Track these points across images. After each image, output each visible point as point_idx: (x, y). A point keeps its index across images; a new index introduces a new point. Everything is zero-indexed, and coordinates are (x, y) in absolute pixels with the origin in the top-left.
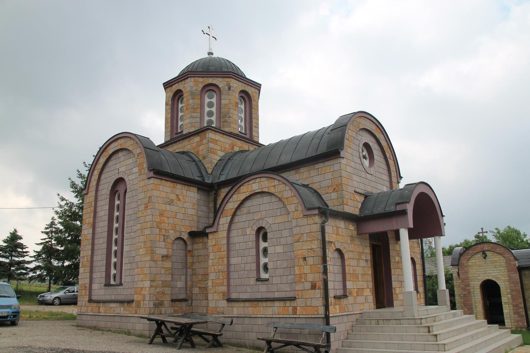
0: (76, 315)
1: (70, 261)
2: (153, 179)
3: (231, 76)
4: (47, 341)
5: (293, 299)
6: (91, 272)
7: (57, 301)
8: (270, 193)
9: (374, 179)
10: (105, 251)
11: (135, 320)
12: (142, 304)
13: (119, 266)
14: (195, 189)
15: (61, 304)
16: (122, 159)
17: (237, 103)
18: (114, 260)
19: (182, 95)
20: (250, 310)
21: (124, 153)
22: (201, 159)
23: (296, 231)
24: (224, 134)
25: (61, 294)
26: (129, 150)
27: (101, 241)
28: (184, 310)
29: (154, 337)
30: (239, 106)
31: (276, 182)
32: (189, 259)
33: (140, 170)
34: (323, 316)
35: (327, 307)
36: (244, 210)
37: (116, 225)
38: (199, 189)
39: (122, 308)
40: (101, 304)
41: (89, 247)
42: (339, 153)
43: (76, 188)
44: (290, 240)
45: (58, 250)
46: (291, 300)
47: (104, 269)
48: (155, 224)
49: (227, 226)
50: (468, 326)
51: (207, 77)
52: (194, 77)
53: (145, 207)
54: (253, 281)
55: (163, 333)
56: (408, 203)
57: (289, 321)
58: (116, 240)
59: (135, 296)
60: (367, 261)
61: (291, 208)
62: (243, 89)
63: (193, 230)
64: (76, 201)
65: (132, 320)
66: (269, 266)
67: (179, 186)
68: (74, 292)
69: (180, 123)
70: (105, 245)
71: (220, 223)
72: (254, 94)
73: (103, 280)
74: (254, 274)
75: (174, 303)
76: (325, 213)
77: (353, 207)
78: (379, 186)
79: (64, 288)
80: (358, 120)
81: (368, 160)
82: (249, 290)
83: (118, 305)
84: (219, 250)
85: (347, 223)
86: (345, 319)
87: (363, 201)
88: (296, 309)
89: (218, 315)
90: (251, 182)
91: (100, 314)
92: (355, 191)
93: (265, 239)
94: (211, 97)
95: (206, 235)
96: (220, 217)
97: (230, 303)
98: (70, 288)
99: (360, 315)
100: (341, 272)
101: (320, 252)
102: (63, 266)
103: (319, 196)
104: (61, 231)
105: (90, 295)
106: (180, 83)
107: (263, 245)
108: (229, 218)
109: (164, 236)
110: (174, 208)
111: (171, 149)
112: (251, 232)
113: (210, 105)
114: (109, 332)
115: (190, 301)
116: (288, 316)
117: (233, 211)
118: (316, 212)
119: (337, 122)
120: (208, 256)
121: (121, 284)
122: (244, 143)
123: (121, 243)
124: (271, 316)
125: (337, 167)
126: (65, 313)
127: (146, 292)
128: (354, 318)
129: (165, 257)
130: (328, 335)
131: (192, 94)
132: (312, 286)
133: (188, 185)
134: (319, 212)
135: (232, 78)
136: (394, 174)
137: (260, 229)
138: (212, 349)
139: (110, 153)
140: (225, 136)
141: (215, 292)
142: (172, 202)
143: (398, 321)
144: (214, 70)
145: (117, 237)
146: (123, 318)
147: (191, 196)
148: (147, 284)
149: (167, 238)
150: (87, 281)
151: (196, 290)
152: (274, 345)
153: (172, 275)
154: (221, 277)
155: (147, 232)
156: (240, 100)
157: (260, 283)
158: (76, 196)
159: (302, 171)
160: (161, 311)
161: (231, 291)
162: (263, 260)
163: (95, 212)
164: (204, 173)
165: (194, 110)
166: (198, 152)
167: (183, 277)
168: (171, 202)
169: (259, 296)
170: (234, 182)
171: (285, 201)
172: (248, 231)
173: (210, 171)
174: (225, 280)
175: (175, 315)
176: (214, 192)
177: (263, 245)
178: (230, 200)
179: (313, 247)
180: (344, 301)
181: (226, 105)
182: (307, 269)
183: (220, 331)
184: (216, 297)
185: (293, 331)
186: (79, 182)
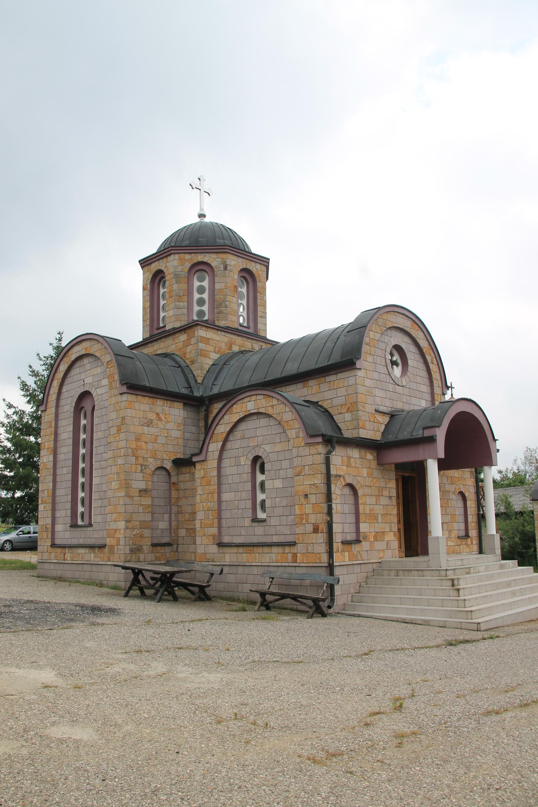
0: (35, 563)
1: (22, 491)
2: (126, 395)
4: (6, 592)
5: (293, 544)
6: (54, 510)
7: (8, 546)
8: (268, 414)
9: (406, 391)
10: (69, 484)
11: (109, 569)
12: (116, 550)
13: (88, 502)
14: (180, 405)
15: (13, 549)
16: (88, 367)
17: (236, 287)
18: (81, 495)
19: (163, 277)
20: (244, 557)
21: (90, 359)
22: (189, 364)
23: (297, 462)
24: (218, 330)
25: (13, 535)
26: (96, 356)
27: (65, 470)
28: (168, 556)
29: (130, 589)
30: (240, 289)
31: (275, 402)
32: (174, 494)
33: (110, 383)
34: (326, 565)
35: (331, 553)
36: (238, 434)
37: (82, 451)
38: (185, 404)
39: (92, 555)
40: (67, 549)
41: (50, 478)
42: (354, 364)
43: (27, 390)
44: (290, 473)
45: (6, 476)
46: (290, 545)
47: (69, 506)
48: (130, 451)
49: (217, 454)
50: (514, 580)
51: (196, 253)
52: (178, 253)
53: (118, 430)
54: (247, 522)
55: (140, 583)
56: (438, 427)
57: (289, 570)
58: (83, 470)
59: (108, 539)
60: (390, 497)
61: (292, 433)
62: (245, 267)
63: (178, 457)
64: (29, 408)
65: (104, 569)
66: (268, 504)
67: (160, 402)
68: (29, 533)
69: (162, 315)
70: (69, 477)
71: (210, 450)
72: (260, 272)
73: (69, 520)
74: (249, 513)
75: (155, 548)
76: (334, 439)
77: (372, 430)
78: (414, 401)
79: (16, 529)
80: (385, 317)
81: (400, 367)
82: (243, 533)
83: (87, 550)
84: (209, 484)
85: (363, 452)
86: (357, 569)
87: (388, 423)
88: (297, 557)
89: (207, 563)
90: (246, 400)
91: (66, 562)
92: (376, 411)
93: (262, 471)
94: (201, 280)
95: (193, 464)
96: (209, 443)
97: (221, 548)
98: (25, 528)
99: (379, 564)
100: (354, 512)
101: (323, 488)
102: (13, 497)
103: (330, 416)
104: (9, 450)
105: (53, 538)
106: (161, 261)
107: (260, 478)
108: (220, 444)
109: (142, 465)
110: (153, 430)
111: (148, 350)
112: (246, 462)
113: (201, 290)
114: (78, 584)
115: (175, 546)
116: (287, 564)
117: (224, 436)
118: (320, 440)
119: (356, 320)
120: (194, 490)
121: (90, 525)
122: (246, 339)
123: (89, 473)
124: (268, 564)
125: (351, 381)
126: (20, 561)
127: (120, 535)
128: (370, 567)
129: (143, 492)
130: (331, 587)
131: (177, 276)
132: (314, 529)
133: (170, 400)
134: (323, 439)
135: (229, 253)
136: (437, 383)
137: (256, 459)
138: (197, 603)
139: (73, 359)
140: (219, 333)
141: (204, 535)
142: (151, 423)
143: (420, 573)
145: (84, 465)
146: (94, 566)
147: (175, 414)
148: (122, 525)
149: (145, 468)
150: (49, 521)
151: (182, 532)
152: (269, 598)
153: (153, 514)
154: (210, 517)
155: (120, 461)
156: (241, 280)
157: (256, 524)
158: (29, 402)
159: (310, 385)
160: (139, 558)
161: (223, 534)
162: (260, 496)
163: (56, 434)
164: (193, 383)
165: (179, 298)
166: (185, 354)
167: (166, 516)
168: (149, 423)
169: (255, 540)
170: (230, 396)
171: (285, 424)
172: (243, 460)
173: (200, 380)
174: (216, 521)
175: (156, 562)
176: (204, 408)
177: (260, 478)
178: (221, 422)
179: (316, 482)
180: (355, 548)
181: (221, 290)
182: (308, 509)
183: (208, 582)
184: (205, 541)
185: (293, 582)
186: (31, 382)
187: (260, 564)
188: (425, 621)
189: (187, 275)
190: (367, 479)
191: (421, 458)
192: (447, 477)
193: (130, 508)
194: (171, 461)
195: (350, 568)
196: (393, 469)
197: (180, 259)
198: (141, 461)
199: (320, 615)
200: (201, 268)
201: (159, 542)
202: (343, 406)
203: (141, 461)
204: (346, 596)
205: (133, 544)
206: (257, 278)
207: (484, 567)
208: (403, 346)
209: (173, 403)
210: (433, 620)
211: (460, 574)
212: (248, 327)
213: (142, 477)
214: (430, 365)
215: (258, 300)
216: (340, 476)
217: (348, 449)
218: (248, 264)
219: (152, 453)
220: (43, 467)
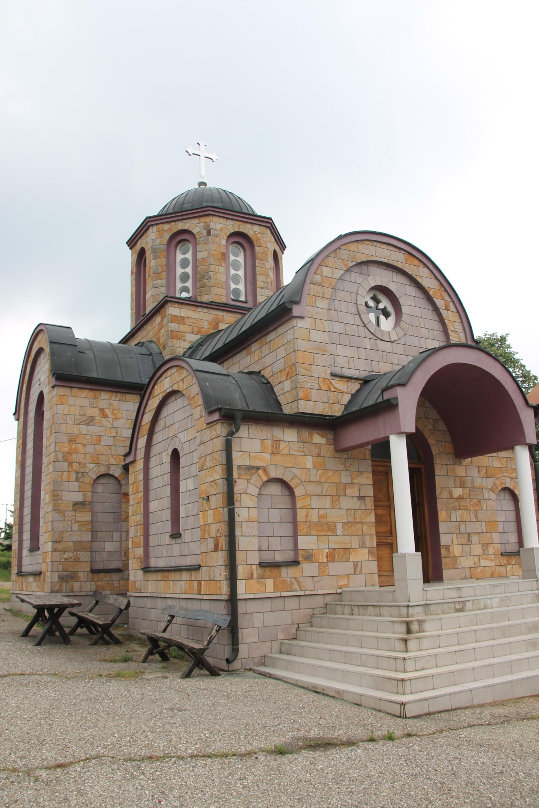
3: (210, 212)
5: (198, 568)
24: (197, 306)
28: (116, 585)
48: (60, 455)
52: (156, 224)
67: (105, 396)
72: (259, 236)
75: (96, 575)
77: (330, 402)
84: (138, 492)
85: (305, 433)
86: (292, 604)
101: (222, 486)
109: (77, 473)
110: (94, 429)
125: (290, 335)
128: (320, 601)
129: (78, 506)
131: (155, 251)
135: (213, 215)
140: (199, 309)
142: (92, 421)
143: (377, 610)
144: (190, 208)
168: (90, 421)
180: (288, 573)
181: (204, 259)
188: (338, 692)
189: (165, 248)
190: (314, 472)
191: (382, 436)
192: (478, 467)
193: (60, 526)
194: (121, 466)
195: (278, 604)
196: (368, 456)
197: (158, 231)
198: (75, 466)
199: (207, 673)
200: (180, 238)
201: (105, 568)
202: (283, 372)
203: (75, 466)
204: (269, 644)
205: (63, 570)
206: (255, 243)
207: (498, 600)
208: (392, 287)
209: (124, 395)
210: (348, 692)
211: (439, 612)
212: (246, 302)
213: (78, 488)
214: (444, 313)
215: (257, 268)
216: (258, 468)
217: (274, 429)
218: (242, 226)
219: (93, 457)
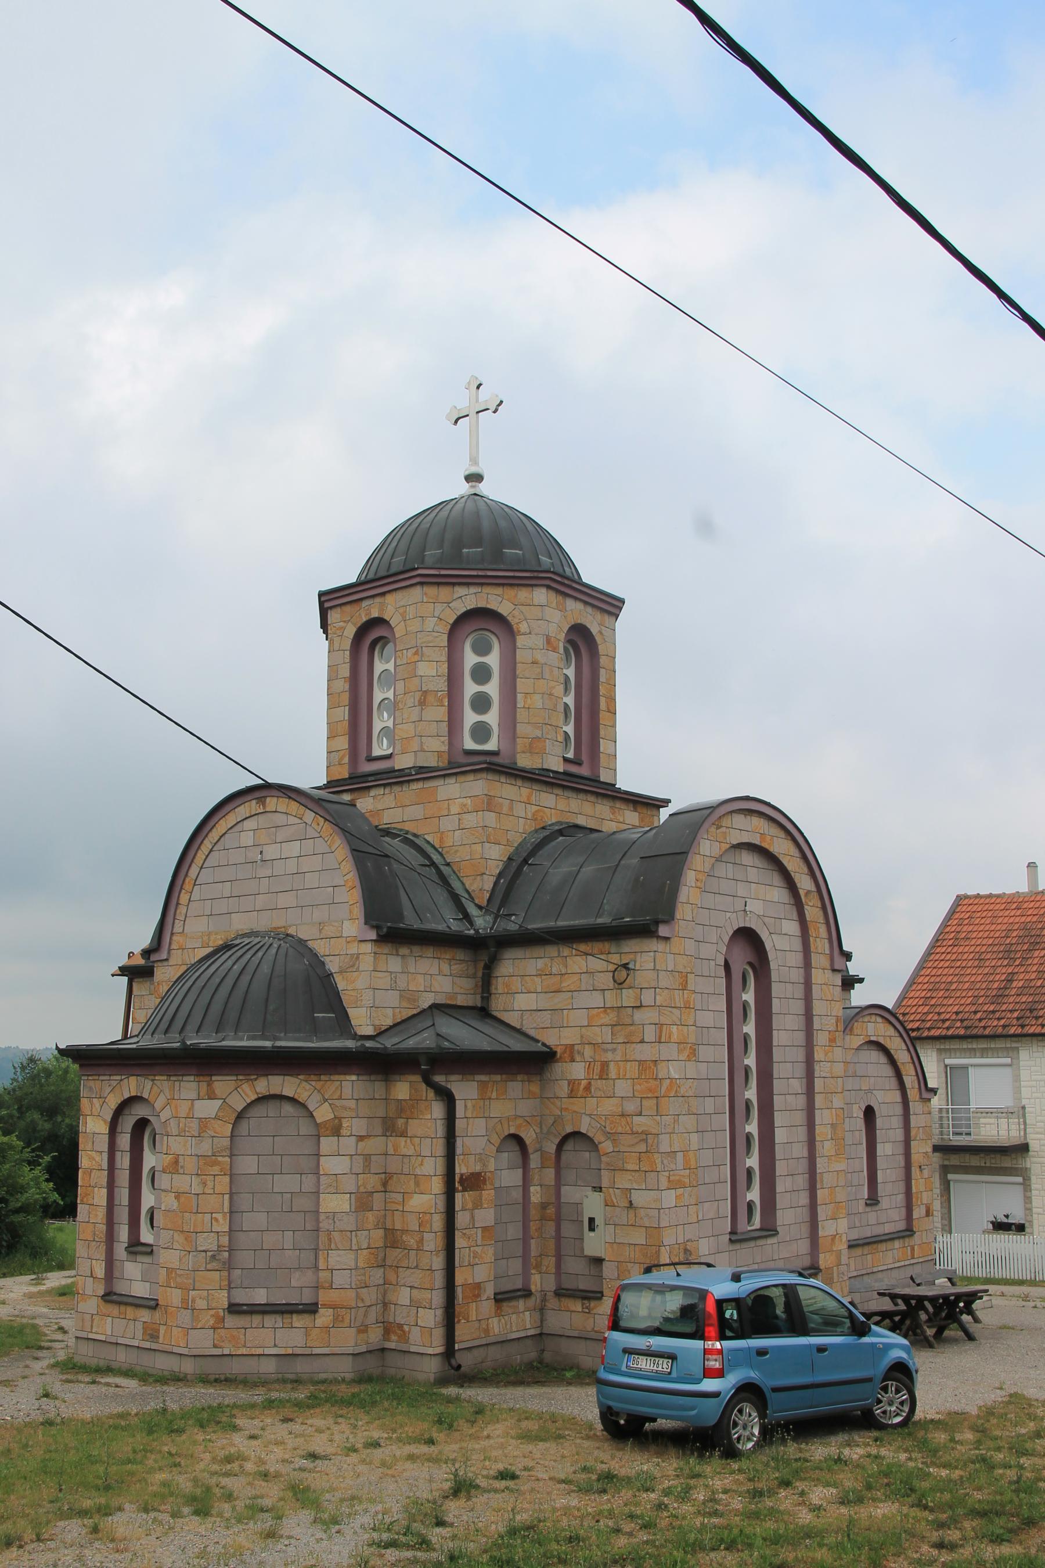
105: (890, 1238)
187: (885, 1267)
220: (668, 1090)
